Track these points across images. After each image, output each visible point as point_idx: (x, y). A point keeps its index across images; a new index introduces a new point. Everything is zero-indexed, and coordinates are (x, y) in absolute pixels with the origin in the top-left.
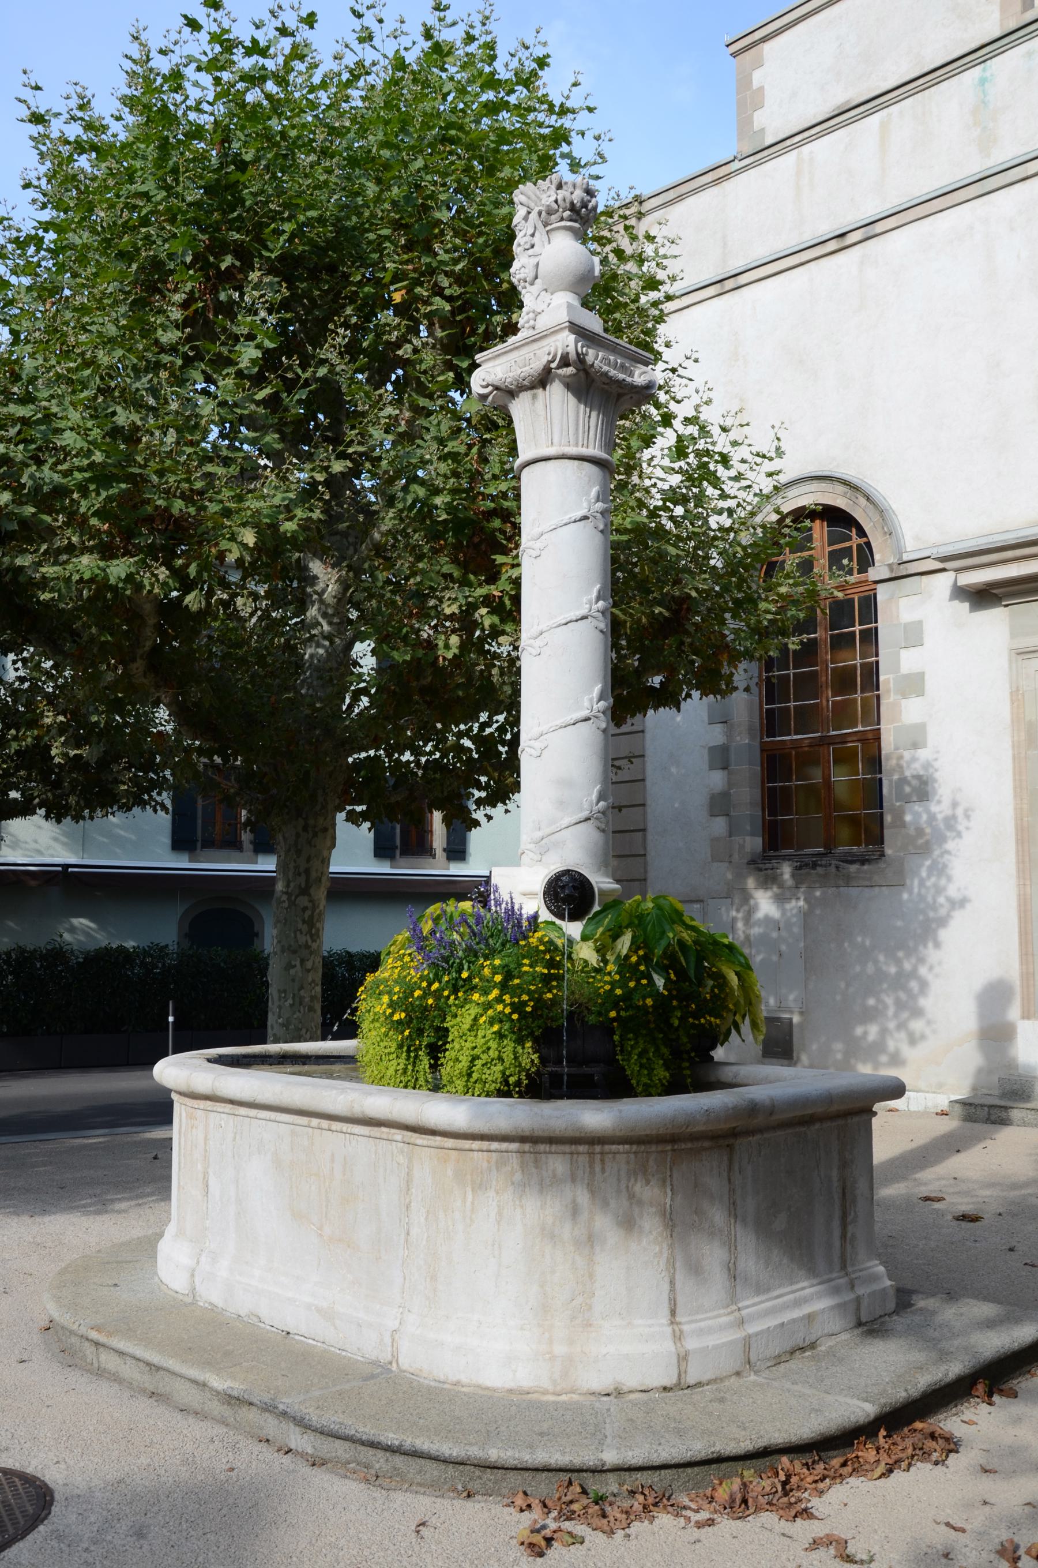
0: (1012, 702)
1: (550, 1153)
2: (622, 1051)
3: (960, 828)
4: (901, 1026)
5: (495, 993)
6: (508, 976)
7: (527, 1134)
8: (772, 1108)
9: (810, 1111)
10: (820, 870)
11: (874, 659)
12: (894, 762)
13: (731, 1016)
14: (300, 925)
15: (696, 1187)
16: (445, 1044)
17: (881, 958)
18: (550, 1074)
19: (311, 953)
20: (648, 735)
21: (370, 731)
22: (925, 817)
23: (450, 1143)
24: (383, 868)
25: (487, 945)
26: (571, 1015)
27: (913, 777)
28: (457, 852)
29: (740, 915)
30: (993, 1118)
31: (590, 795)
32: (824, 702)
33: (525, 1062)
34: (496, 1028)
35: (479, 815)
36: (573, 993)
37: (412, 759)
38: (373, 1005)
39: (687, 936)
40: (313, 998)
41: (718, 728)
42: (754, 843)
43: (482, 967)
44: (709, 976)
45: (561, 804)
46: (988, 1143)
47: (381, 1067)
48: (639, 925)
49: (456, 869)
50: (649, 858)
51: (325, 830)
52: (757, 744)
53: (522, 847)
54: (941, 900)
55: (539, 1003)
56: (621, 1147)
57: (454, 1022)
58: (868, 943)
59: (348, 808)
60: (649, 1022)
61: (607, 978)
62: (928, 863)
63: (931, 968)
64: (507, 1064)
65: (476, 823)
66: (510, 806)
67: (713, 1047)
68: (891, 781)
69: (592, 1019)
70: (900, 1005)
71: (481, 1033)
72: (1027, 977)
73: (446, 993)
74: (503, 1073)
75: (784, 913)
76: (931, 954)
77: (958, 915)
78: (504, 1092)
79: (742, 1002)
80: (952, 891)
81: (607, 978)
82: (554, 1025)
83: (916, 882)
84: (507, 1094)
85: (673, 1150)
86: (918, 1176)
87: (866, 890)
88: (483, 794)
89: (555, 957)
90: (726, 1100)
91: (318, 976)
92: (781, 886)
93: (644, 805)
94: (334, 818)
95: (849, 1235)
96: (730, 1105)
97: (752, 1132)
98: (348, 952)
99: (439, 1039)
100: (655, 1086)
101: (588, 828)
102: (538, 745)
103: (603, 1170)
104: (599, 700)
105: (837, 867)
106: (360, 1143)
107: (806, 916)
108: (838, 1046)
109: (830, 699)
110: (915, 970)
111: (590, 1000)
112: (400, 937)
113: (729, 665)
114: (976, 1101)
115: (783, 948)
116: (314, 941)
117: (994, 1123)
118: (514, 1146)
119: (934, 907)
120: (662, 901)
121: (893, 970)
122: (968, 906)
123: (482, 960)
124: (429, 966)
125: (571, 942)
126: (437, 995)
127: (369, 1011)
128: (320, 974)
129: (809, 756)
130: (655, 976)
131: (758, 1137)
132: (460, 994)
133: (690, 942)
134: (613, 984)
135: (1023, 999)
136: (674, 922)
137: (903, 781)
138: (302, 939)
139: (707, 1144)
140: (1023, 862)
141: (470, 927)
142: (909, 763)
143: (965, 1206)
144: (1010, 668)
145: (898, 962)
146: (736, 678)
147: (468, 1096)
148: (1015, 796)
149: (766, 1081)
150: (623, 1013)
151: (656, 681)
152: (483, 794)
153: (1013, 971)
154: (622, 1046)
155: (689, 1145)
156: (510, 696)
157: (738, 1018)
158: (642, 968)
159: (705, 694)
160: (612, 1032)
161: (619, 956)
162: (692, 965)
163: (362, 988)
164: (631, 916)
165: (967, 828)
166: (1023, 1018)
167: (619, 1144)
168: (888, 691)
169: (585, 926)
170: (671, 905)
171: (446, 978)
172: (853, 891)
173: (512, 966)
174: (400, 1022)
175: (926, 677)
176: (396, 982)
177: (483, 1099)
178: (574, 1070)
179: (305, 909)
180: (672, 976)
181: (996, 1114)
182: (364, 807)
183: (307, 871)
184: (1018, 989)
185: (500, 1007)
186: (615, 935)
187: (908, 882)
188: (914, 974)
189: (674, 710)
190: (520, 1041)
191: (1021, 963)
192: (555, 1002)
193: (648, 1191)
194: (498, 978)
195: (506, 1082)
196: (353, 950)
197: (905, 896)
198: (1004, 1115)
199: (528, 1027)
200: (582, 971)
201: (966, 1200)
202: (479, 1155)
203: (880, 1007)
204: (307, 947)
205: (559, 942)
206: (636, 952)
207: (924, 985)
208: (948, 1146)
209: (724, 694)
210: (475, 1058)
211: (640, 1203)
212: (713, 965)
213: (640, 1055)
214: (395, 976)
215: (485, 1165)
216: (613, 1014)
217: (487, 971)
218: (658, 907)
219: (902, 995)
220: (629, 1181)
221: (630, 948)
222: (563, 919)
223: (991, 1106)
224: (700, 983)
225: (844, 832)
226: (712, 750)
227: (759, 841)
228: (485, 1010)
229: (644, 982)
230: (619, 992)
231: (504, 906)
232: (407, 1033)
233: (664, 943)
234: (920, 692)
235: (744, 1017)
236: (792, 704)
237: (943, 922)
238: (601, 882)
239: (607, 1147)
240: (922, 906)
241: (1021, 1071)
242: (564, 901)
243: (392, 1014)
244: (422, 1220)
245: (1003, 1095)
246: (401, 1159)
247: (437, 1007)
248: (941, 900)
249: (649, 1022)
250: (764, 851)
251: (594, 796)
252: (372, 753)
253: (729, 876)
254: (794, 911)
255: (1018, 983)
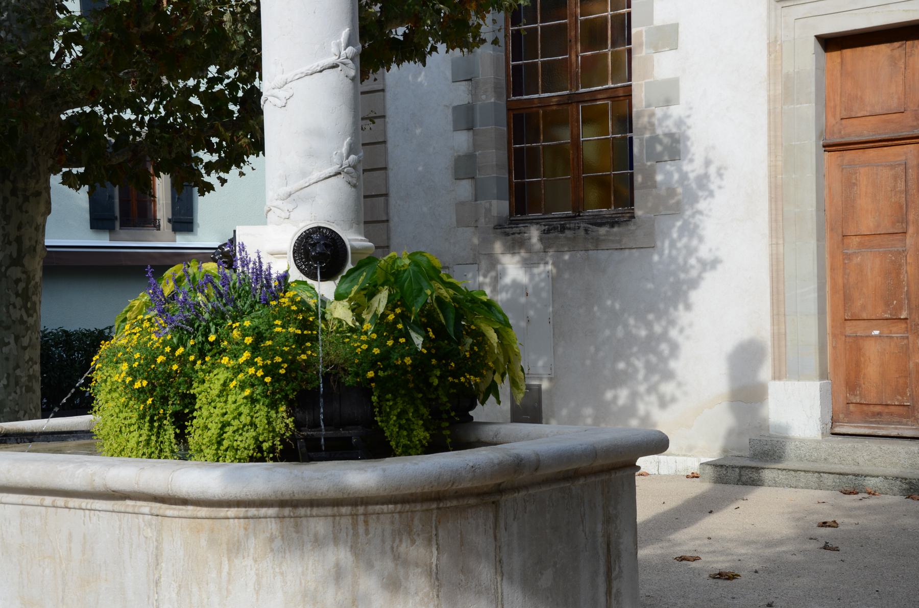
0: (770, 54)
1: (312, 516)
2: (380, 412)
3: (712, 187)
4: (652, 389)
5: (246, 355)
6: (259, 337)
7: (287, 497)
8: (537, 463)
9: (575, 466)
10: (568, 233)
11: (626, 10)
12: (645, 119)
13: (490, 373)
14: (13, 299)
15: (462, 545)
16: (192, 412)
17: (632, 321)
18: (306, 438)
19: (27, 329)
20: (389, 95)
21: (91, 81)
22: (676, 176)
23: (203, 511)
24: (102, 240)
25: (235, 307)
26: (326, 376)
27: (666, 135)
28: (184, 221)
29: (488, 280)
30: (744, 479)
31: (341, 147)
32: (573, 57)
33: (279, 427)
34: (247, 392)
35: (212, 179)
36: (328, 354)
37: (133, 117)
38: (110, 377)
39: (445, 293)
40: (30, 378)
41: (463, 87)
42: (500, 207)
43: (231, 329)
44: (468, 334)
45: (311, 155)
46: (740, 503)
47: (122, 438)
48: (396, 282)
49: (182, 241)
50: (392, 224)
51: (38, 194)
52: (503, 103)
53: (268, 203)
54: (693, 261)
55: (293, 364)
56: (385, 507)
57: (202, 388)
58: (617, 306)
59: (64, 170)
60: (408, 381)
61: (364, 338)
62: (679, 223)
63: (681, 331)
64: (260, 430)
65: (209, 187)
66: (246, 168)
67: (473, 406)
68: (641, 140)
69: (349, 380)
70: (650, 369)
71: (231, 399)
72: (779, 337)
73: (192, 358)
74: (256, 439)
75: (532, 277)
76: (683, 316)
77: (708, 276)
78: (258, 455)
79: (502, 359)
80: (704, 252)
81: (364, 338)
82: (309, 388)
83: (667, 243)
84: (262, 460)
85: (438, 508)
86: (672, 537)
87: (616, 253)
88: (215, 158)
89: (308, 317)
90: (491, 456)
91: (37, 354)
92: (529, 251)
93: (385, 169)
94: (47, 181)
95: (614, 591)
96: (496, 461)
97: (516, 489)
98: (65, 332)
99: (186, 407)
100: (415, 447)
101: (339, 182)
102: (282, 94)
103: (367, 532)
104: (347, 46)
105: (586, 230)
106: (102, 520)
107: (554, 280)
108: (588, 411)
109: (578, 55)
110: (665, 333)
111: (346, 360)
112: (137, 303)
113: (477, 13)
114: (727, 463)
115: (532, 313)
116: (30, 315)
117: (744, 484)
118: (272, 511)
119: (685, 268)
120: (418, 258)
121: (643, 333)
122: (719, 267)
123: (230, 323)
124: (172, 330)
125: (324, 302)
126: (182, 360)
127: (106, 381)
128: (38, 352)
129: (557, 116)
130: (414, 335)
131: (523, 493)
132: (207, 359)
133: (448, 299)
134: (370, 343)
135: (774, 359)
136: (432, 279)
137: (655, 139)
138: (16, 314)
139: (472, 501)
140: (776, 221)
141: (215, 287)
142: (661, 121)
143: (722, 565)
144: (769, 17)
145: (649, 325)
146: (483, 29)
147: (221, 463)
148: (770, 153)
149: (528, 437)
150: (381, 373)
151: (400, 32)
152: (215, 158)
153: (764, 331)
154: (380, 408)
155: (455, 503)
156: (244, 47)
157: (497, 378)
158: (400, 326)
159: (451, 47)
160: (370, 393)
161: (375, 315)
162: (452, 322)
163: (97, 357)
164: (386, 272)
165: (720, 187)
166: (774, 378)
167: (383, 504)
168: (641, 45)
169: (338, 288)
170: (429, 261)
171: (192, 342)
172: (602, 255)
173: (263, 328)
174: (141, 390)
175: (680, 29)
176: (135, 348)
177: (236, 464)
178: (331, 434)
179: (18, 281)
180: (431, 334)
181: (747, 474)
182: (82, 170)
183: (19, 240)
184: (769, 350)
185: (251, 371)
186: (371, 293)
187: (659, 244)
188: (664, 337)
189: (419, 64)
190: (273, 405)
191: (773, 324)
192: (309, 364)
193: (417, 551)
194: (249, 340)
195: (259, 448)
196: (71, 328)
197: (656, 258)
198: (755, 476)
199: (282, 390)
200: (337, 332)
201: (721, 559)
202: (232, 523)
203: (630, 370)
204: (22, 322)
205: (312, 302)
206: (393, 310)
207: (675, 348)
208: (702, 507)
209: (470, 47)
210: (225, 425)
211: (406, 563)
212: (473, 323)
213: (399, 416)
214: (134, 342)
215: (242, 532)
216: (371, 374)
217: (236, 334)
218: (415, 263)
219: (653, 359)
220: (394, 542)
221: (387, 307)
222: (315, 279)
223: (742, 468)
224: (460, 342)
225: (593, 195)
226: (456, 109)
227: (505, 205)
228: (236, 375)
229: (402, 340)
230: (376, 351)
231: (251, 265)
232: (149, 401)
233: (421, 300)
234: (674, 47)
235: (503, 376)
236: (539, 60)
237: (694, 284)
238: (353, 239)
239: (371, 508)
240: (673, 267)
241: (772, 432)
242: (315, 259)
243: (132, 383)
244: (174, 595)
245: (754, 457)
246: (149, 532)
247: (182, 373)
248: (693, 261)
249: (408, 381)
250: (511, 215)
251: (344, 149)
252: (88, 109)
253: (476, 241)
254: (543, 276)
255: (769, 343)
